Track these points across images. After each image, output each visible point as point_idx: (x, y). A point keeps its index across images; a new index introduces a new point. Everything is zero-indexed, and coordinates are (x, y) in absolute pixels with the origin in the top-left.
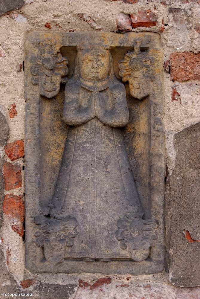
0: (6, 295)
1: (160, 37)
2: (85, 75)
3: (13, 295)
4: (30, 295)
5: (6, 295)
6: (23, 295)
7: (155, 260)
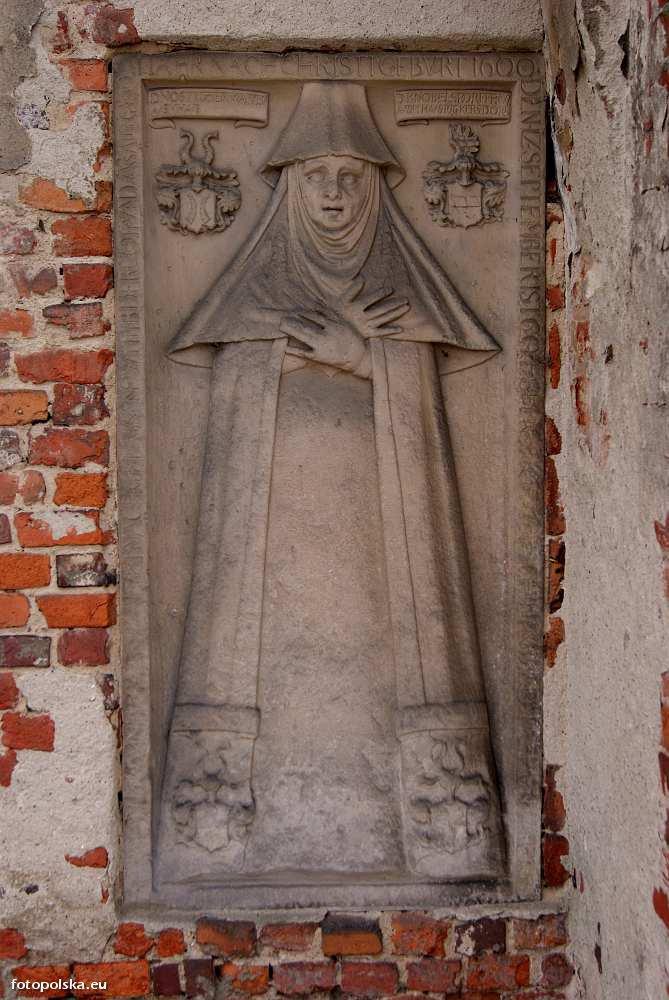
0: (21, 985)
1: (204, 804)
2: (547, 575)
3: (45, 985)
4: (101, 987)
5: (21, 985)
6: (76, 985)
7: (208, 795)
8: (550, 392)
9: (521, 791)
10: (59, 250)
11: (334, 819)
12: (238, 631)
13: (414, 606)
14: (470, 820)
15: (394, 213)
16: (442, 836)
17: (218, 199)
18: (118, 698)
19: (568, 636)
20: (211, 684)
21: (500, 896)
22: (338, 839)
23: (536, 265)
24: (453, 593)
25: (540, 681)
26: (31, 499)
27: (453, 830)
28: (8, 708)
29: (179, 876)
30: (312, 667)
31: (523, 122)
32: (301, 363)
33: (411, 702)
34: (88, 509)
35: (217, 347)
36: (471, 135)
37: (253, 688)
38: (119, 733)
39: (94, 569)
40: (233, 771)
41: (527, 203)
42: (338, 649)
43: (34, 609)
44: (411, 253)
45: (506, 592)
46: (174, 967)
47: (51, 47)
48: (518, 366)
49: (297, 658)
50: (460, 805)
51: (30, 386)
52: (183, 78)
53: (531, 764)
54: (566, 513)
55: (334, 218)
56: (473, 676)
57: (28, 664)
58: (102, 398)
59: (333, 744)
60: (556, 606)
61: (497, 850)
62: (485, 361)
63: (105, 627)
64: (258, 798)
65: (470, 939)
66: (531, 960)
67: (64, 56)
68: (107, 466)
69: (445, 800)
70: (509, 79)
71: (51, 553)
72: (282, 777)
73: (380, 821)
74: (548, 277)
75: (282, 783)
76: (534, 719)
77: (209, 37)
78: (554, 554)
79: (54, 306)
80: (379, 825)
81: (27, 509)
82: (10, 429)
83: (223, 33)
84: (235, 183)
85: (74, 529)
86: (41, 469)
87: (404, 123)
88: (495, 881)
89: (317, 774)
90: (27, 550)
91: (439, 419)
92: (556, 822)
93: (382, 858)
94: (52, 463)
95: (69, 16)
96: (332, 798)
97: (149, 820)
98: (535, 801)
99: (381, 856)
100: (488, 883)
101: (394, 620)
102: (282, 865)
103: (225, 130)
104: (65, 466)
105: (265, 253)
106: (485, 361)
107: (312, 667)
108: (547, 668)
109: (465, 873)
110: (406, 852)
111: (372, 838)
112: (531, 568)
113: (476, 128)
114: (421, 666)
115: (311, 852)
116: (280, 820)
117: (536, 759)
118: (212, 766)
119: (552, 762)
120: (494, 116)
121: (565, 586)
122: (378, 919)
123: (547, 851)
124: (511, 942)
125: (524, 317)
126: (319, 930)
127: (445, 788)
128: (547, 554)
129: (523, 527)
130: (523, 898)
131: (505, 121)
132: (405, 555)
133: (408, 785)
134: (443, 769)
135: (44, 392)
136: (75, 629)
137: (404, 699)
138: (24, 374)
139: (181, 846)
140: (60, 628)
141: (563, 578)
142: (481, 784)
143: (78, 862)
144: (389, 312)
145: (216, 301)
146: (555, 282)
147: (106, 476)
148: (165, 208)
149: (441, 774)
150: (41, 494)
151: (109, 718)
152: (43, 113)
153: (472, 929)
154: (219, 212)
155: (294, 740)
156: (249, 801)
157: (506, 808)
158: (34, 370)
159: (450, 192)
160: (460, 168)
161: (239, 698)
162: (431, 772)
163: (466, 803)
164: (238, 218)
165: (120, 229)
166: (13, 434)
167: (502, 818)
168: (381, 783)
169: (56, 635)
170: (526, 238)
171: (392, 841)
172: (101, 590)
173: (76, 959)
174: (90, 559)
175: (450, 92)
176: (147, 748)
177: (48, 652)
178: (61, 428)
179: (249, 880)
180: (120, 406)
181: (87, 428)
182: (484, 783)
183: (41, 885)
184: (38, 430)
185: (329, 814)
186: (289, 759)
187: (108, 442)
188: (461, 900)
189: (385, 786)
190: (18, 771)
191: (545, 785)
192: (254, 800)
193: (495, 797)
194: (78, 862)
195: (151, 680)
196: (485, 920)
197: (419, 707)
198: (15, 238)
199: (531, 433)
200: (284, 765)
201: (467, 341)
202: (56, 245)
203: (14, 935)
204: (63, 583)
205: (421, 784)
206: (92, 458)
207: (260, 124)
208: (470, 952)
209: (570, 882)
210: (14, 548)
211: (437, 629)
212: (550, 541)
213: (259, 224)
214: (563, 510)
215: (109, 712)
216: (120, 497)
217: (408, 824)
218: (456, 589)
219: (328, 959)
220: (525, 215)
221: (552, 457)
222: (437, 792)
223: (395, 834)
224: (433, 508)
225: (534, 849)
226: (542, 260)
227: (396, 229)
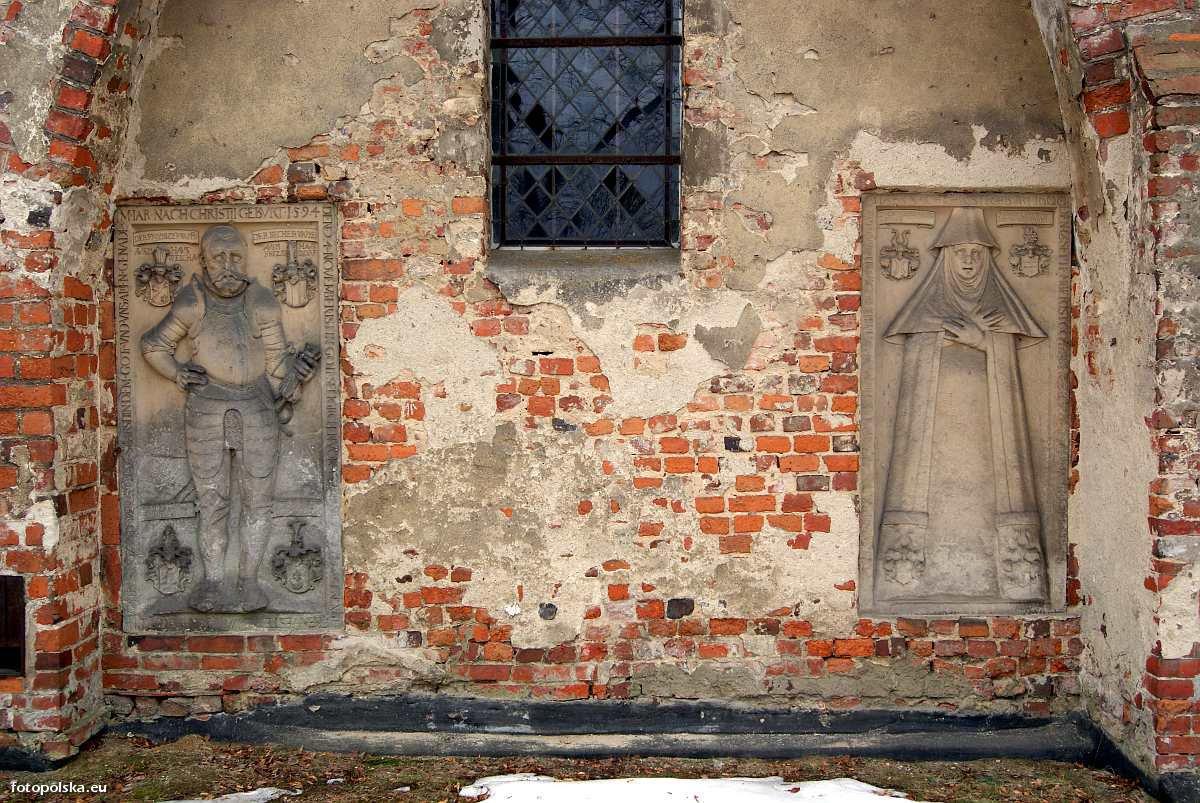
3: (45, 788)
5: (21, 788)
8: (1073, 358)
12: (918, 474)
15: (995, 269)
19: (1081, 478)
25: (1067, 501)
26: (821, 408)
29: (887, 597)
33: (1003, 511)
44: (1004, 289)
51: (821, 354)
59: (964, 531)
61: (1045, 587)
67: (840, 195)
69: (1020, 560)
71: (830, 435)
75: (939, 550)
86: (824, 394)
100: (1040, 603)
103: (913, 229)
105: (933, 289)
109: (1029, 598)
111: (983, 579)
112: (1062, 445)
118: (904, 542)
121: (1080, 454)
124: (1052, 632)
138: (818, 348)
145: (908, 312)
162: (1012, 546)
168: (988, 551)
169: (832, 475)
170: (1061, 283)
180: (863, 364)
190: (812, 542)
204: (836, 450)
206: (851, 389)
208: (1032, 637)
209: (1081, 603)
210: (812, 432)
211: (1016, 474)
217: (1001, 572)
222: (1015, 556)
223: (994, 577)
224: (1015, 415)
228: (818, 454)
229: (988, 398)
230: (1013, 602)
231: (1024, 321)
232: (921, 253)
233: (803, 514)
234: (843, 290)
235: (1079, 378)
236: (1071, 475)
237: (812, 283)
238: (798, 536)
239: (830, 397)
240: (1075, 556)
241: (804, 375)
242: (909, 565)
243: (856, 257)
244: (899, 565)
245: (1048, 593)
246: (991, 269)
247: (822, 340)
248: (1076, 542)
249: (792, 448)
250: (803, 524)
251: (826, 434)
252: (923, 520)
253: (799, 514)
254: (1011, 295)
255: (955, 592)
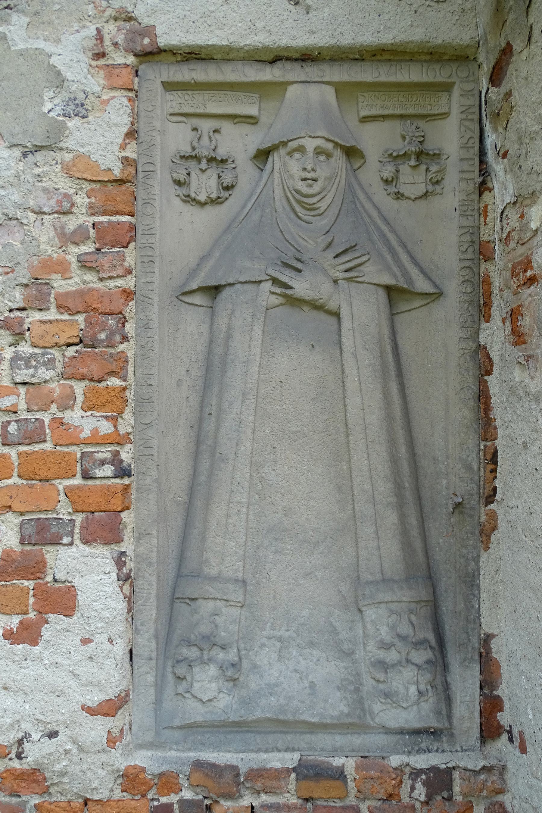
8: (484, 325)
9: (463, 656)
10: (92, 210)
11: (307, 677)
12: (228, 516)
13: (374, 497)
14: (420, 680)
15: (357, 187)
16: (397, 693)
17: (219, 177)
18: (130, 570)
19: (502, 525)
20: (207, 560)
21: (446, 746)
22: (310, 694)
23: (472, 225)
24: (405, 488)
25: (477, 563)
26: (63, 408)
27: (407, 689)
28: (39, 578)
29: (177, 722)
30: (288, 547)
31: (462, 112)
32: (281, 300)
33: (371, 578)
34: (109, 414)
35: (216, 290)
36: (417, 128)
37: (241, 563)
38: (130, 600)
39: (112, 463)
40: (223, 634)
41: (464, 176)
42: (311, 533)
43: (62, 497)
44: (370, 217)
45: (447, 488)
46: (172, 805)
47: (90, 54)
48: (458, 304)
49: (276, 540)
50: (413, 667)
51: (66, 317)
52: (193, 81)
53: (471, 633)
54: (498, 423)
55: (310, 186)
56: (421, 558)
57: (56, 542)
58: (123, 326)
59: (305, 613)
60: (490, 500)
61: (443, 706)
62: (429, 303)
63: (120, 512)
64: (243, 657)
65: (422, 786)
66: (474, 805)
67: (102, 62)
68: (125, 380)
69: (399, 663)
70: (450, 81)
71: (77, 451)
72: (264, 640)
73: (345, 680)
74: (482, 234)
75: (263, 645)
76: (474, 595)
77: (213, 46)
78: (489, 457)
79: (86, 253)
80: (344, 683)
81: (60, 415)
82: (49, 350)
83: (225, 43)
84: (233, 166)
85: (97, 430)
86: (72, 383)
87: (365, 120)
88: (441, 731)
89: (291, 638)
90: (58, 448)
91: (393, 347)
92: (492, 683)
93: (347, 712)
94: (82, 379)
95: (105, 32)
96: (305, 659)
97: (154, 674)
98: (475, 665)
99: (346, 710)
100: (435, 733)
101: (357, 509)
102: (263, 715)
103: (226, 126)
104: (92, 380)
105: (256, 216)
106: (429, 303)
107: (288, 547)
108: (482, 551)
109: (416, 725)
110: (366, 706)
111: (338, 694)
112: (469, 468)
113: (421, 124)
114: (379, 548)
115: (287, 705)
116: (262, 676)
117: (473, 629)
118: (205, 629)
119: (489, 631)
120: (437, 112)
121: (498, 483)
122: (343, 765)
123: (484, 708)
124: (457, 789)
125: (463, 265)
126: (293, 776)
127: (399, 653)
128: (482, 457)
129: (462, 435)
130: (464, 748)
131: (445, 115)
132: (365, 455)
133: (369, 648)
134: (399, 636)
135: (77, 321)
136: (95, 513)
137: (365, 576)
138: (61, 308)
139: (180, 697)
140: (83, 512)
141: (496, 477)
142: (429, 649)
143: (91, 711)
144: (335, 180)
145: (216, 254)
146: (486, 238)
147: (125, 389)
148: (178, 183)
149: (396, 641)
150: (71, 402)
151: (121, 588)
152: (82, 105)
153: (424, 777)
154: (221, 188)
155: (274, 608)
156: (236, 659)
157: (448, 669)
158: (70, 304)
159: (401, 172)
160: (409, 153)
161: (228, 573)
162: (388, 639)
163: (416, 665)
164: (236, 192)
165: (141, 195)
166: (51, 354)
167: (445, 676)
168: (346, 646)
169: (79, 519)
170: (463, 203)
171: (355, 697)
172: (118, 481)
173: (88, 797)
174: (108, 455)
175: (402, 93)
176: (154, 613)
177: (72, 533)
178: (89, 350)
179: (236, 727)
180: (138, 335)
181: (109, 350)
182: (431, 647)
183: (61, 730)
184: (71, 351)
185: (302, 673)
186: (269, 625)
187: (126, 361)
188: (412, 748)
189: (349, 649)
190: (46, 632)
191: (482, 650)
192: (240, 658)
193: (440, 659)
194: (91, 711)
195: (158, 556)
196: (434, 769)
197: (378, 582)
198: (58, 200)
199: (468, 357)
200: (265, 630)
201: (414, 286)
202: (91, 206)
203: (38, 774)
204: (86, 476)
205: (380, 648)
206: (113, 373)
207: (251, 120)
208: (423, 798)
209: (505, 737)
210: (48, 446)
211: (392, 518)
212: (485, 446)
213: (251, 195)
214: (495, 420)
215: (121, 582)
216: (136, 406)
217: (368, 684)
218: (407, 485)
219: (300, 801)
220: (463, 185)
221: (486, 378)
222: (392, 656)
223: (357, 690)
224: (389, 417)
225: (474, 706)
226: (477, 221)
227: (358, 199)
228: (56, 482)
229: (344, 390)
230: (388, 731)
231: (401, 266)
232: (238, 162)
233: (30, 584)
234: (104, 213)
235: (495, 359)
236: (483, 518)
237: (53, 202)
238: (21, 622)
239: (79, 387)
240: (494, 655)
241: (37, 351)
242: (212, 670)
243: (126, 160)
244: (196, 670)
245: (450, 717)
246: (349, 187)
247: (68, 294)
248: (496, 632)
249: (15, 474)
250: (31, 601)
251: (71, 449)
252: (236, 594)
253: (26, 583)
254: (384, 227)
255: (290, 717)
